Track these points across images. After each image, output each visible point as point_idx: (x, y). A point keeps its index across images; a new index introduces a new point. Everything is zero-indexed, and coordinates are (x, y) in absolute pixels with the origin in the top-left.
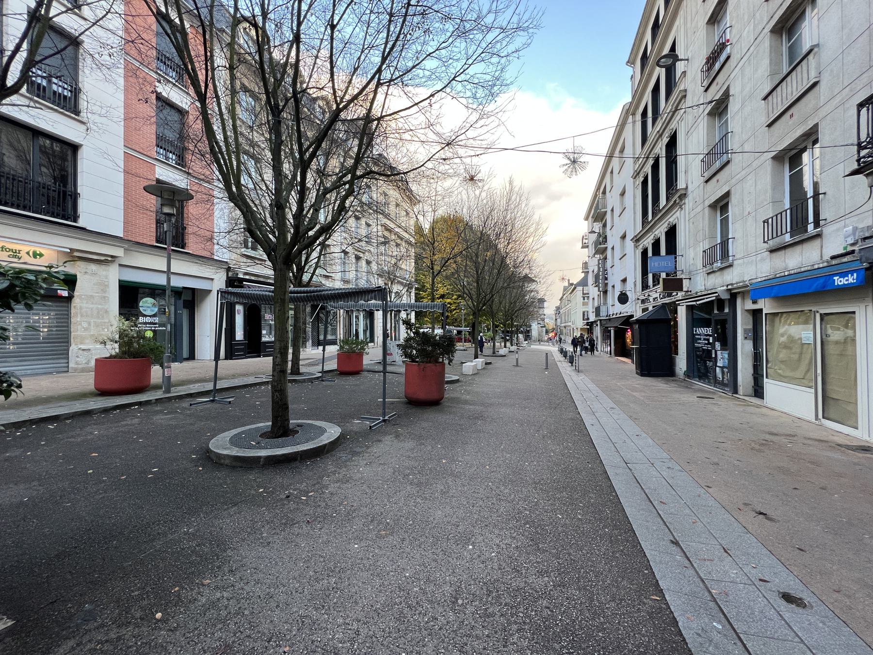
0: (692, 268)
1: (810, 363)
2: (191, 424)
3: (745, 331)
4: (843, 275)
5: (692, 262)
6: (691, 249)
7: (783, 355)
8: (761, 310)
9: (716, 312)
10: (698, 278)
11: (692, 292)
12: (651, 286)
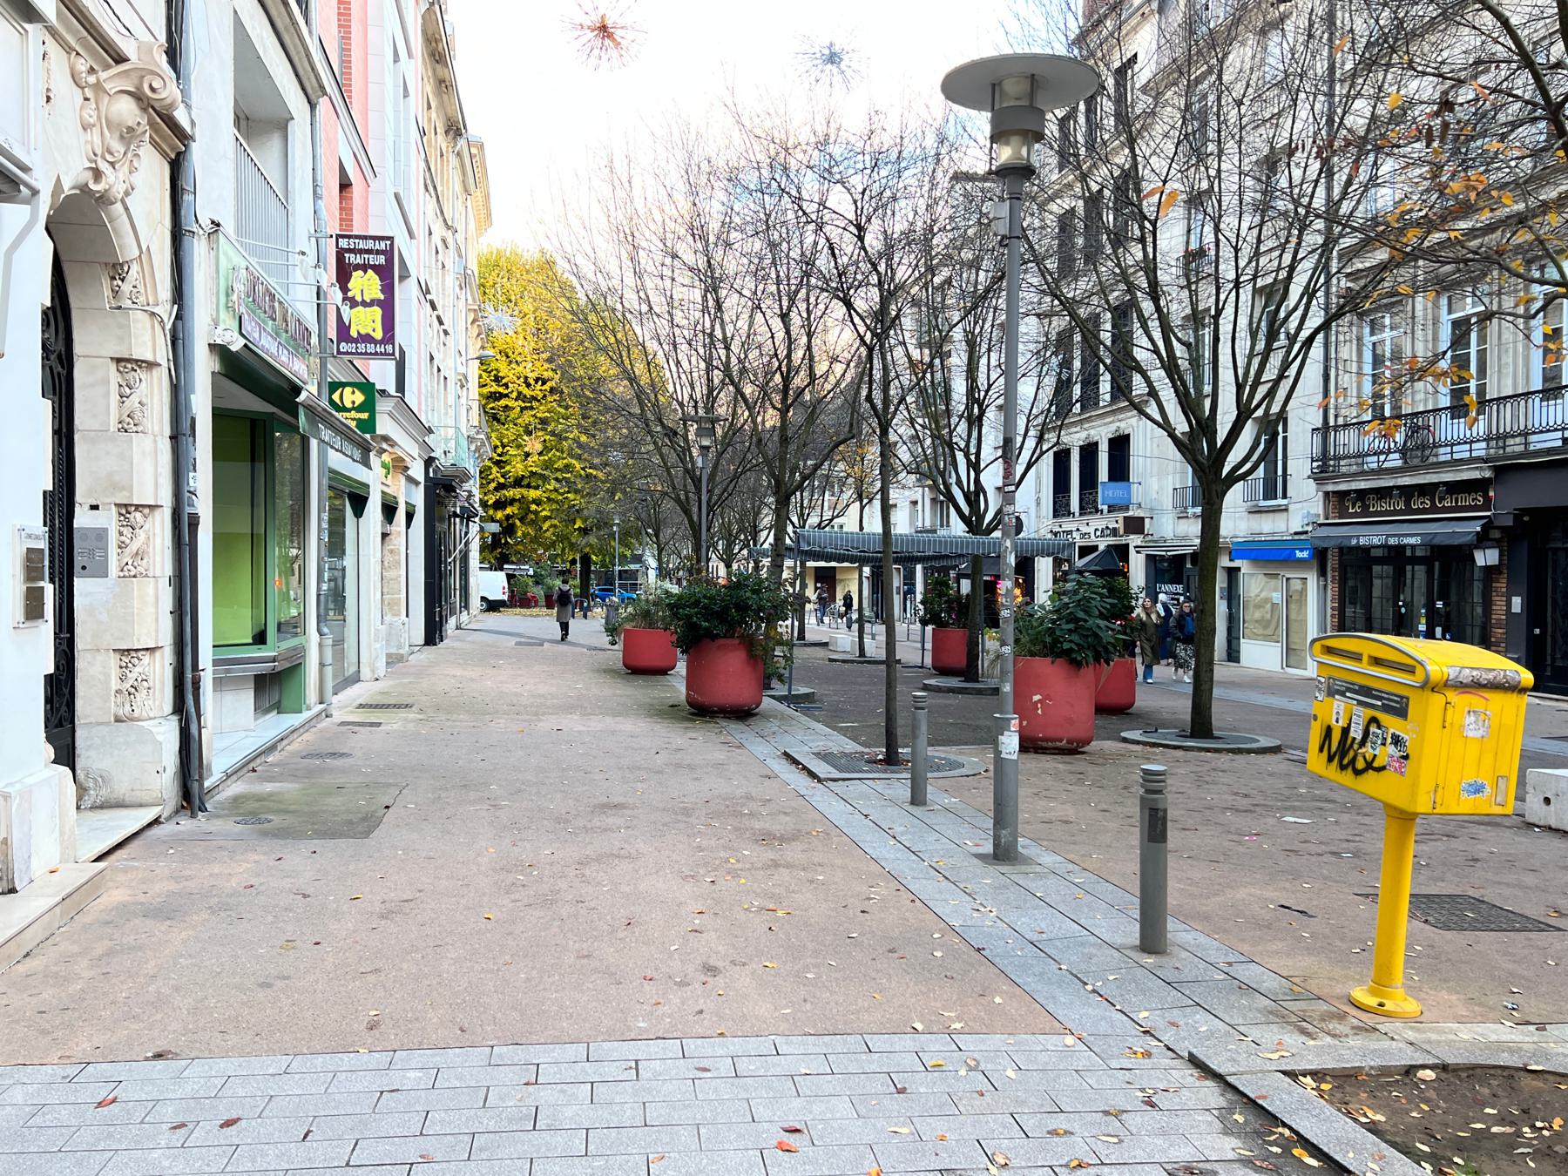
0: (1154, 504)
1: (347, 73)
2: (472, 680)
3: (1221, 588)
4: (1301, 550)
5: (1155, 496)
6: (1154, 479)
7: (1257, 615)
8: (1238, 569)
9: (1189, 566)
10: (1164, 520)
11: (1156, 537)
12: (1077, 514)
